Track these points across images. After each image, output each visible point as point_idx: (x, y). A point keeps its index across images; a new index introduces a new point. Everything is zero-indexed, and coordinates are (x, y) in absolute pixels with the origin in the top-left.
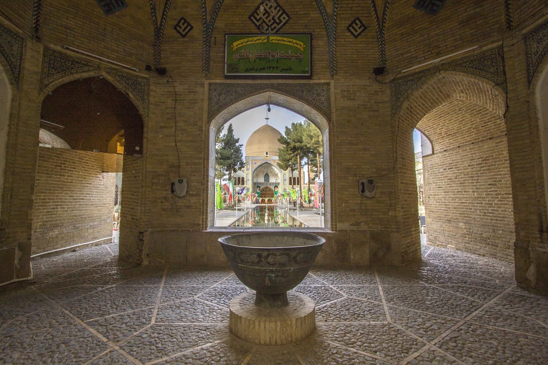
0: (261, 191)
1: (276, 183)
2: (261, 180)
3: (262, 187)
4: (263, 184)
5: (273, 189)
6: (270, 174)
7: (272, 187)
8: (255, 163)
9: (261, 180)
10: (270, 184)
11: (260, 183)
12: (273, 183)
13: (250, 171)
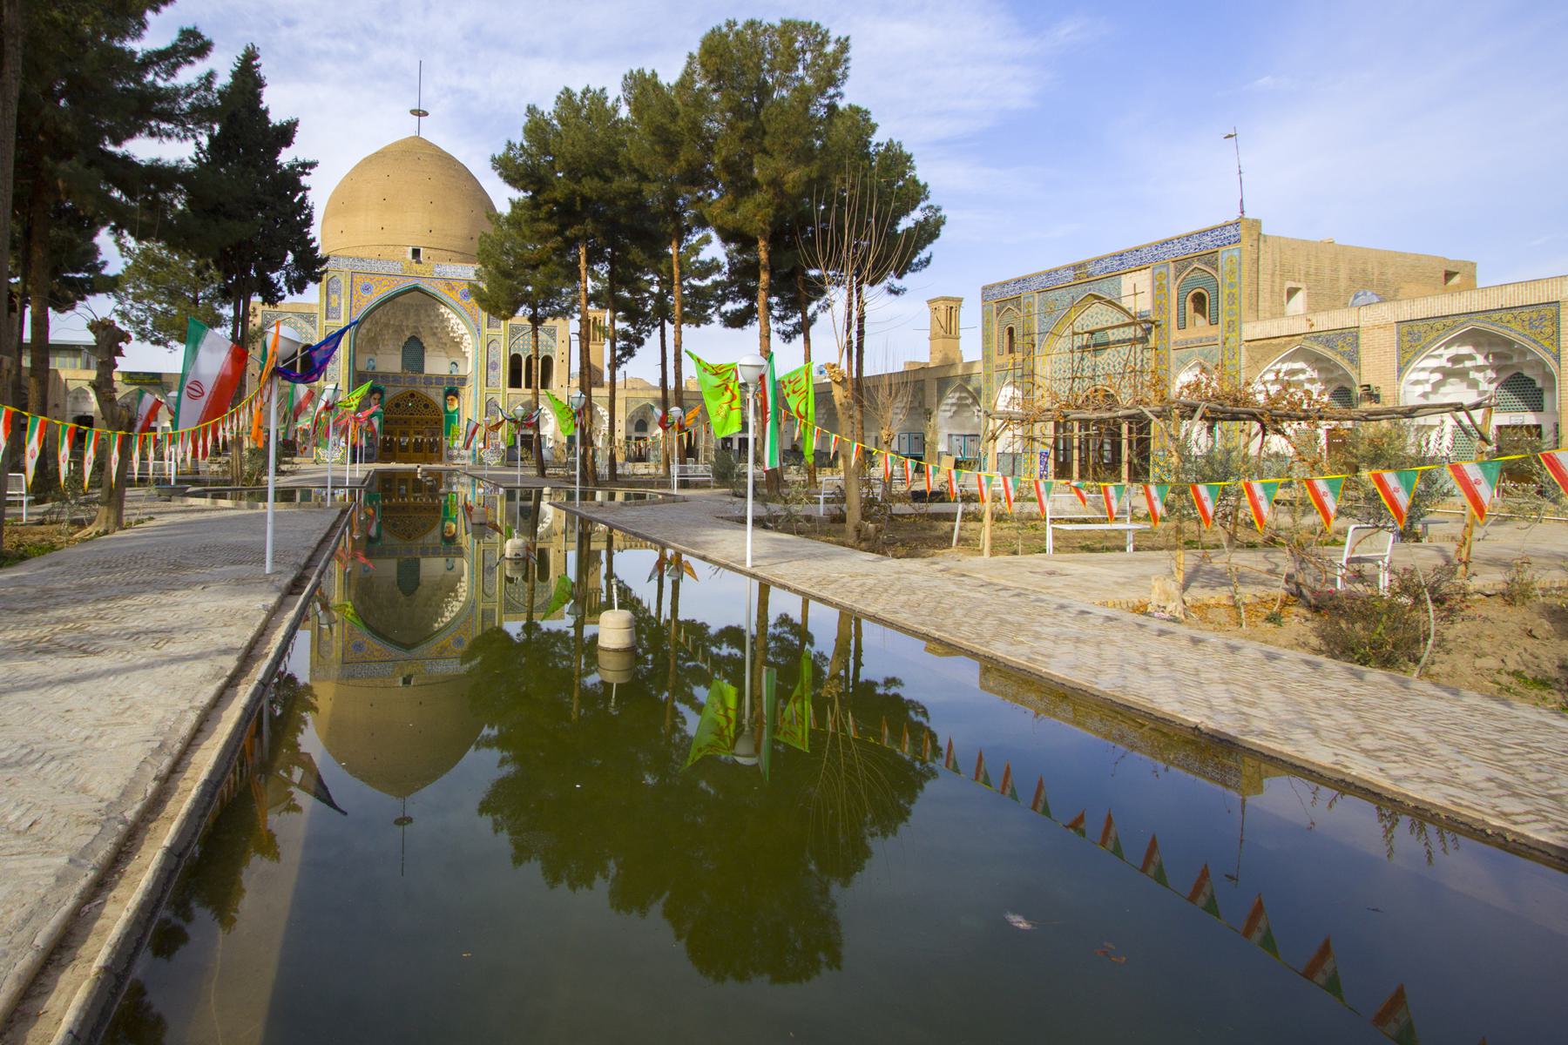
1: (451, 379)
2: (391, 362)
4: (395, 378)
5: (439, 400)
6: (428, 341)
7: (436, 395)
8: (367, 289)
9: (391, 362)
10: (429, 380)
11: (385, 376)
12: (439, 379)
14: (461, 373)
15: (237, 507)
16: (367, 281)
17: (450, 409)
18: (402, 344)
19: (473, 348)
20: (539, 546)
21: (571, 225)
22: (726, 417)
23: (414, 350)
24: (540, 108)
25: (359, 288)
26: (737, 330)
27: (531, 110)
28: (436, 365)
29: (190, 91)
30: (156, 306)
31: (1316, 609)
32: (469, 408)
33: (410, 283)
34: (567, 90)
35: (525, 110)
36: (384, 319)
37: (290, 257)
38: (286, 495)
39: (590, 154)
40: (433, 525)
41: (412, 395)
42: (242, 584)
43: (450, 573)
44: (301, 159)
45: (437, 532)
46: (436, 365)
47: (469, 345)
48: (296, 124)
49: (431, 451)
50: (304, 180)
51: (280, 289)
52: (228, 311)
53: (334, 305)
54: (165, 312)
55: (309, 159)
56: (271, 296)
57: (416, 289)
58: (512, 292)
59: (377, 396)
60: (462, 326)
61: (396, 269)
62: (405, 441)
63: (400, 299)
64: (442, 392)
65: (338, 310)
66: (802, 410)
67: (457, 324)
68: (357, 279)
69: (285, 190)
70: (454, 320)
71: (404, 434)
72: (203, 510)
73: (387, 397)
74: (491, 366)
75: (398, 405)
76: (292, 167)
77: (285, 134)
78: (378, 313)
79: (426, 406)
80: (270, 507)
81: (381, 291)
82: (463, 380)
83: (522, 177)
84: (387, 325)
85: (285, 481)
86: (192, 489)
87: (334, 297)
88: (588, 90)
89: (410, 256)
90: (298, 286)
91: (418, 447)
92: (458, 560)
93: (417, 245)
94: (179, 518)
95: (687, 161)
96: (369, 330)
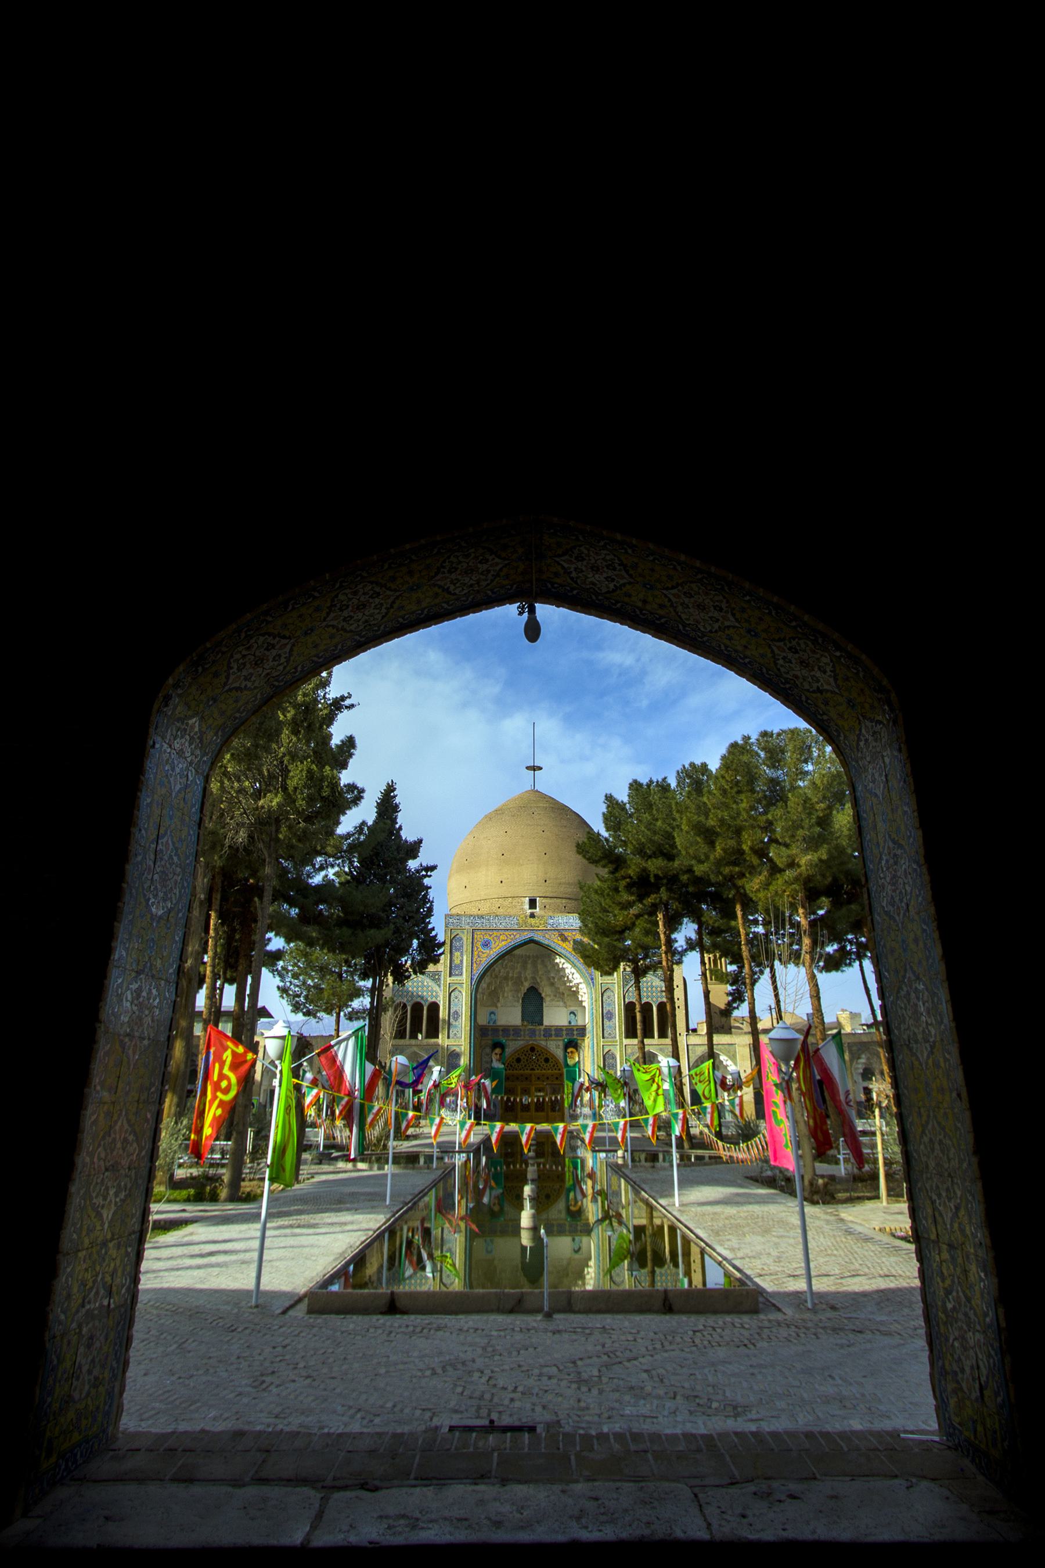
0: (509, 1066)
1: (570, 1029)
2: (511, 1015)
3: (513, 1046)
4: (516, 1031)
5: (559, 1053)
6: (546, 991)
7: (555, 1047)
8: (486, 944)
9: (511, 1015)
11: (506, 1030)
12: (559, 1030)
13: (465, 978)
14: (580, 1023)
15: (371, 1169)
16: (487, 937)
17: (570, 1062)
18: (521, 995)
19: (591, 998)
20: (635, 1041)
21: (648, 895)
22: (655, 1101)
23: (533, 1002)
24: (616, 796)
25: (479, 944)
26: (834, 973)
27: (609, 799)
28: (556, 1016)
29: (348, 835)
30: (310, 982)
31: (311, 1146)
32: (588, 1063)
33: (526, 936)
34: (635, 781)
35: (603, 798)
36: (503, 973)
37: (415, 942)
38: (398, 1159)
39: (651, 841)
40: (558, 1196)
41: (533, 1049)
42: (373, 1209)
43: (577, 1256)
44: (424, 864)
45: (561, 1205)
46: (556, 1016)
47: (585, 994)
48: (420, 841)
49: (553, 1110)
50: (426, 881)
51: (407, 970)
52: (368, 983)
53: (457, 961)
54: (316, 987)
55: (431, 864)
56: (400, 977)
57: (531, 941)
58: (611, 949)
59: (498, 1051)
60: (577, 975)
61: (513, 924)
62: (526, 1100)
63: (517, 952)
64: (561, 1044)
65: (460, 966)
66: (706, 1093)
67: (574, 973)
68: (478, 936)
69: (414, 894)
70: (569, 969)
71: (526, 1092)
72: (346, 1172)
73: (508, 1051)
74: (607, 1016)
75: (518, 1060)
76: (418, 871)
77: (413, 849)
78: (497, 967)
79: (547, 1060)
80: (389, 1169)
81: (499, 946)
82: (582, 1031)
83: (601, 859)
84: (506, 978)
85: (405, 1146)
86: (335, 1154)
87: (457, 954)
88: (651, 781)
89: (527, 906)
90: (420, 967)
91: (540, 1106)
92: (585, 1239)
93: (532, 895)
94: (331, 1177)
95: (723, 849)
96: (489, 985)
